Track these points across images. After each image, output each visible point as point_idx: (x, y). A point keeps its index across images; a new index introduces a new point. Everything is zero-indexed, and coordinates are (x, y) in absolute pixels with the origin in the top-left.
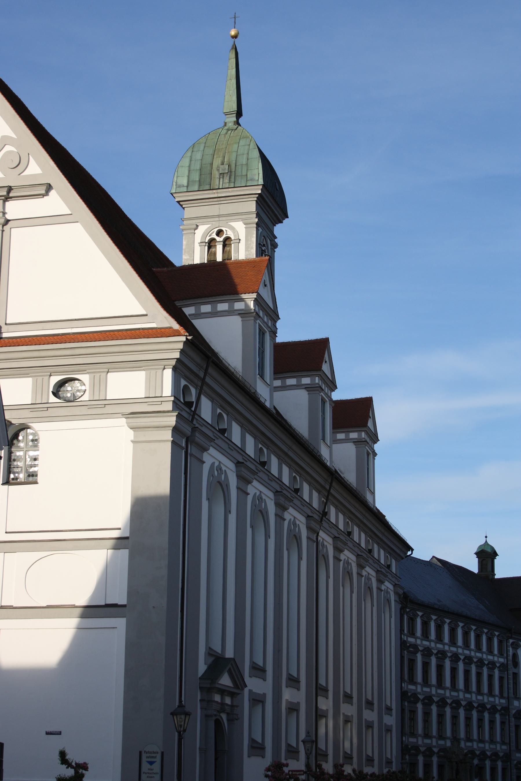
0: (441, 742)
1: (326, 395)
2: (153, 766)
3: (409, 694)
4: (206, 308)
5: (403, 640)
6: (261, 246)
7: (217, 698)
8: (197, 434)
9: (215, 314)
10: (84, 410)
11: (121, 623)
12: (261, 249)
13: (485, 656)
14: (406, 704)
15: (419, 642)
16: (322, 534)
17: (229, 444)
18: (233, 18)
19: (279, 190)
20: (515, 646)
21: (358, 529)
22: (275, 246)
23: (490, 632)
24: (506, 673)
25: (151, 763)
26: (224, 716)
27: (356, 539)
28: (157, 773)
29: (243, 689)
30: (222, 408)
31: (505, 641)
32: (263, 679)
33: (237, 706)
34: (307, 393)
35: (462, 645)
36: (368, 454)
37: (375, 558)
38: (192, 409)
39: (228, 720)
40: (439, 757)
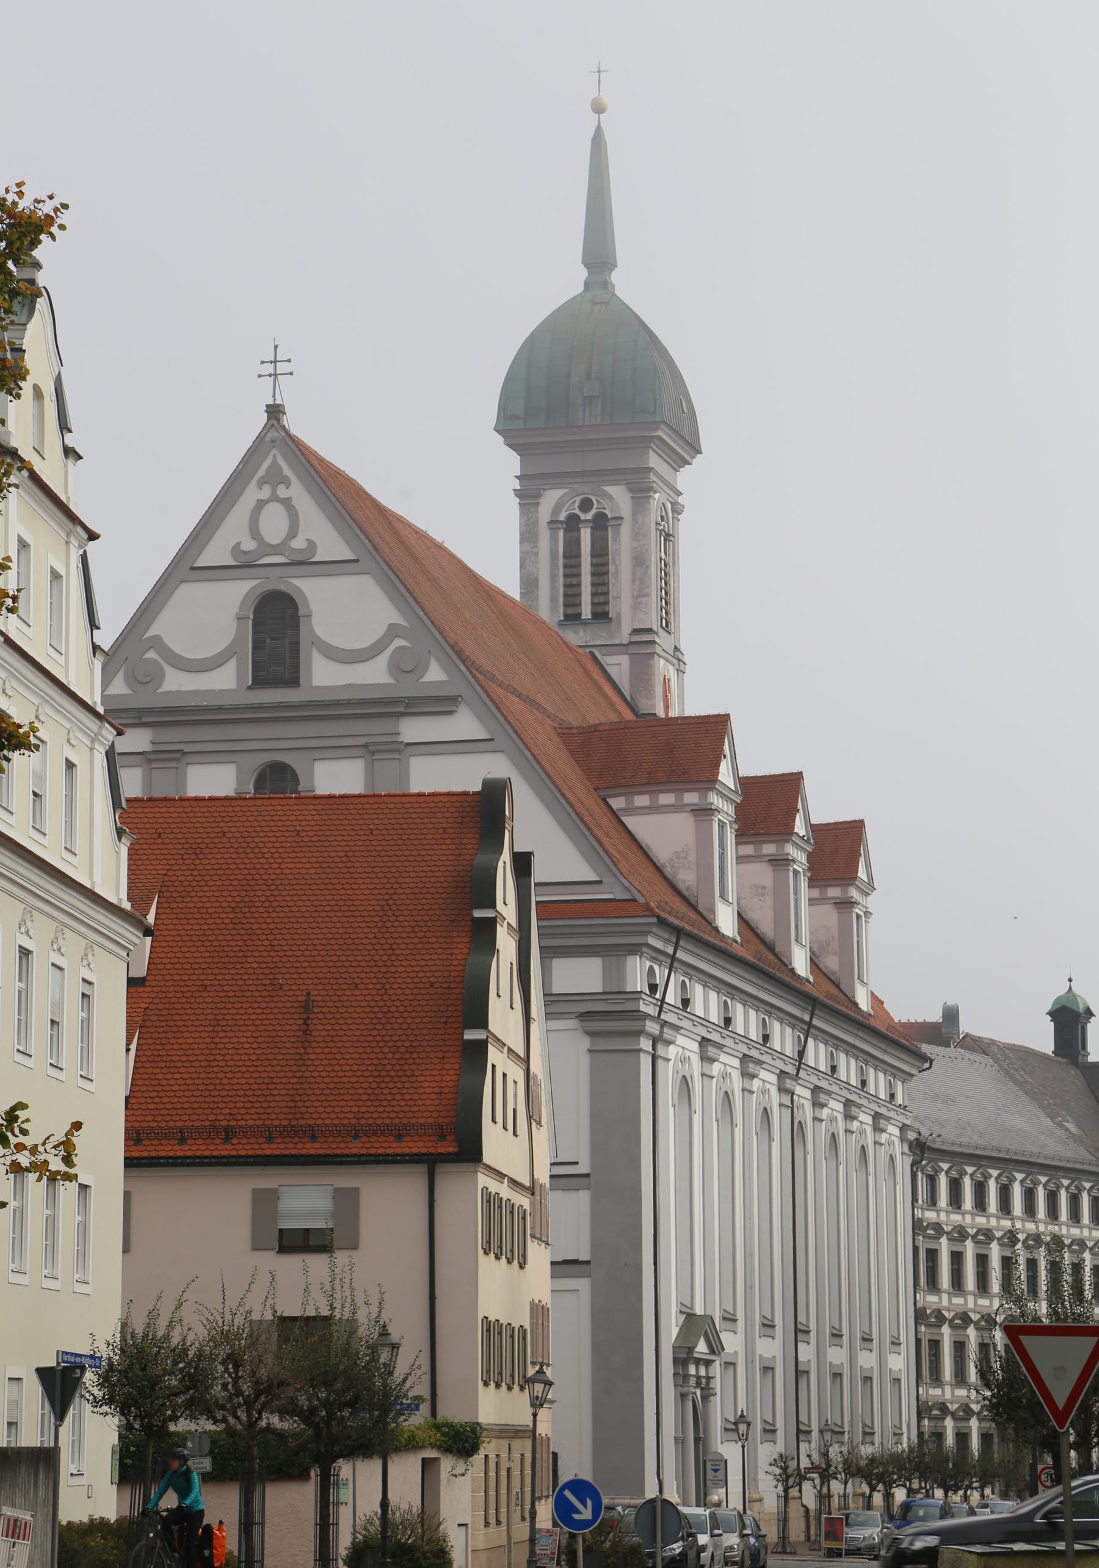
2: (717, 1474)
3: (928, 1312)
4: (642, 800)
9: (655, 809)
15: (943, 1217)
18: (594, 72)
19: (685, 411)
23: (1076, 1183)
25: (716, 1471)
36: (858, 917)
39: (702, 1397)
40: (980, 1420)
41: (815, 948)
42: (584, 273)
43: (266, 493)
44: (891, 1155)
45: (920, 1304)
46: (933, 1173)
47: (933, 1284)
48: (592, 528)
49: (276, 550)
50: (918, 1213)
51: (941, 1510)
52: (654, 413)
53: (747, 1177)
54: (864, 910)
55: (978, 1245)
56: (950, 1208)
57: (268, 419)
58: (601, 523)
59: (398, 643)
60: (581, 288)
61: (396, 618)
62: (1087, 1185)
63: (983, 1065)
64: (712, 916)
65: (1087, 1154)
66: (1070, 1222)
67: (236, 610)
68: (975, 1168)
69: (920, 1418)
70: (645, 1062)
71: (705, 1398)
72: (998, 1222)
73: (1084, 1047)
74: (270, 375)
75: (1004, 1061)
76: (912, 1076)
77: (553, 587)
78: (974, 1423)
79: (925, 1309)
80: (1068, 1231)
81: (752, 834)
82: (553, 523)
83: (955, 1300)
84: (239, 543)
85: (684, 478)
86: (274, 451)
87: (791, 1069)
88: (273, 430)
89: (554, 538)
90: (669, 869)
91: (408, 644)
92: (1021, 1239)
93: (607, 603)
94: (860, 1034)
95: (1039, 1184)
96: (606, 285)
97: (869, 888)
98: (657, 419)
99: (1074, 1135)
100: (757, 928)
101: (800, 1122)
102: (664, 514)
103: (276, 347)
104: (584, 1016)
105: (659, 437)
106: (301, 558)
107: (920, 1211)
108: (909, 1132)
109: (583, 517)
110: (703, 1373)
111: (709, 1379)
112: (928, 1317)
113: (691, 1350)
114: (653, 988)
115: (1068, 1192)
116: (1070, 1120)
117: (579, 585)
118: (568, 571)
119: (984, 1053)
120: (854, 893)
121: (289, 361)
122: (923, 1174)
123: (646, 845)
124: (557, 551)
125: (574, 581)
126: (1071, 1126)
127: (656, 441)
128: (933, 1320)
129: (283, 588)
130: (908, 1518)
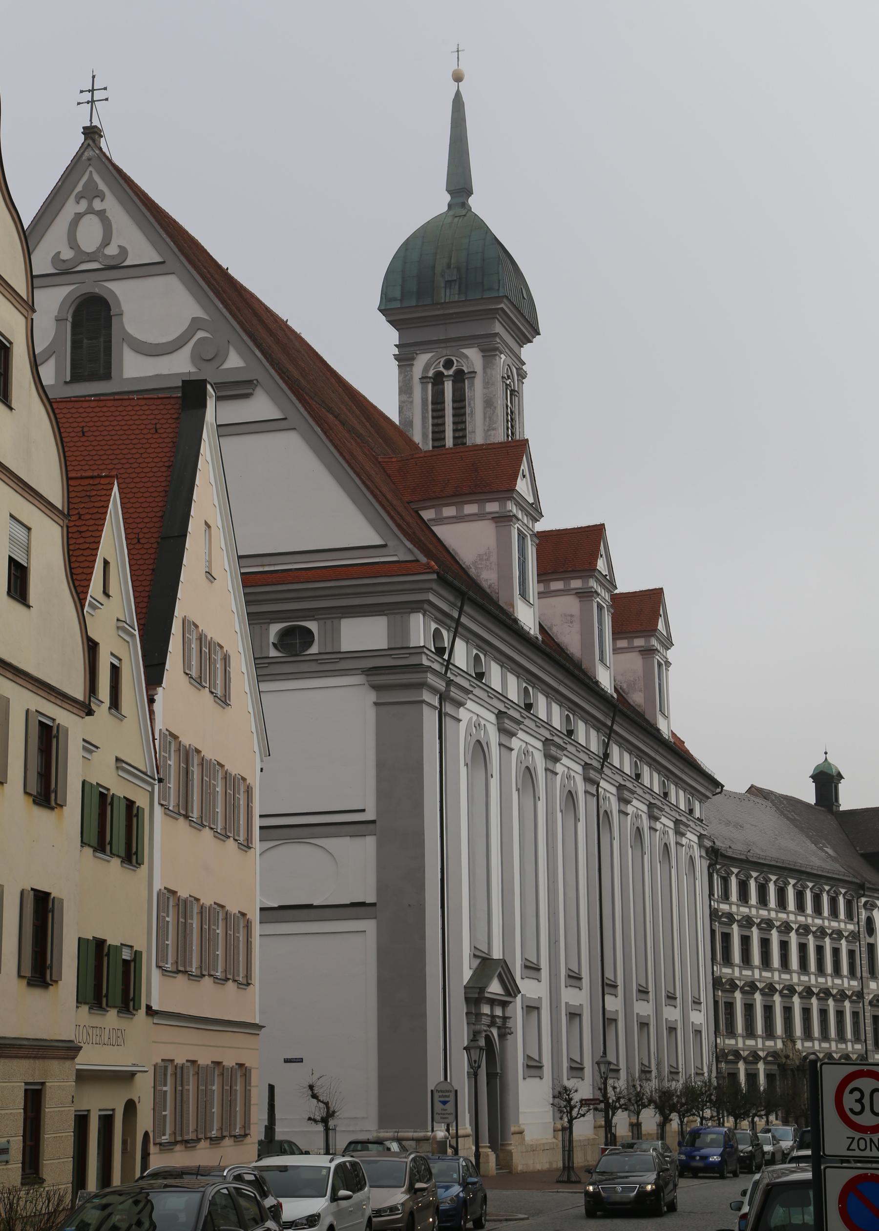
0: (770, 1043)
1: (603, 600)
3: (724, 980)
4: (449, 511)
5: (713, 908)
6: (505, 380)
7: (486, 1009)
8: (452, 689)
10: (314, 667)
11: (369, 926)
12: (504, 384)
13: (826, 923)
14: (720, 993)
15: (734, 909)
16: (603, 784)
17: (488, 692)
18: (455, 52)
20: (870, 907)
21: (649, 768)
22: (522, 375)
24: (858, 944)
25: (444, 1103)
26: (495, 1032)
27: (647, 782)
28: (452, 1114)
29: (516, 996)
30: (478, 647)
31: (856, 901)
32: (538, 980)
33: (510, 1018)
34: (578, 600)
35: (794, 910)
36: (660, 665)
37: (673, 804)
38: (444, 657)
39: (499, 1035)
40: (766, 1063)
41: (619, 678)
42: (447, 198)
43: (83, 206)
44: (691, 856)
45: (717, 974)
46: (726, 875)
47: (727, 960)
48: (453, 381)
49: (91, 257)
50: (715, 905)
51: (724, 1137)
52: (498, 290)
53: (550, 847)
54: (665, 660)
55: (761, 932)
56: (739, 903)
57: (85, 139)
58: (460, 377)
59: (201, 334)
60: (445, 208)
61: (199, 313)
62: (843, 891)
63: (764, 806)
64: (511, 610)
65: (843, 870)
66: (831, 918)
67: (56, 313)
68: (758, 874)
69: (718, 1061)
70: (430, 718)
71: (502, 1036)
72: (777, 915)
73: (837, 800)
74: (88, 102)
75: (780, 805)
76: (708, 798)
77: (424, 427)
78: (761, 1066)
79: (721, 978)
80: (829, 924)
81: (562, 572)
82: (424, 379)
83: (745, 972)
84: (59, 253)
85: (527, 352)
86: (91, 169)
87: (595, 764)
88: (89, 149)
89: (424, 390)
90: (473, 570)
91: (211, 337)
92: (795, 928)
93: (465, 436)
94: (660, 750)
95: (807, 888)
96: (464, 205)
97: (668, 643)
98: (501, 295)
99: (831, 856)
100: (567, 649)
101: (606, 811)
102: (510, 374)
103: (94, 77)
104: (369, 672)
105: (502, 309)
106: (113, 263)
107: (716, 903)
108: (705, 840)
109: (446, 373)
110: (498, 1012)
111: (505, 1018)
112: (723, 984)
113: (482, 990)
114: (440, 651)
115: (828, 895)
116: (829, 847)
117: (444, 424)
118: (435, 414)
119: (765, 798)
120: (654, 642)
121: (105, 89)
122: (718, 875)
123: (453, 550)
124: (427, 400)
125: (440, 421)
126: (830, 851)
127: (500, 312)
128: (728, 987)
129: (97, 290)
130: (697, 1145)
